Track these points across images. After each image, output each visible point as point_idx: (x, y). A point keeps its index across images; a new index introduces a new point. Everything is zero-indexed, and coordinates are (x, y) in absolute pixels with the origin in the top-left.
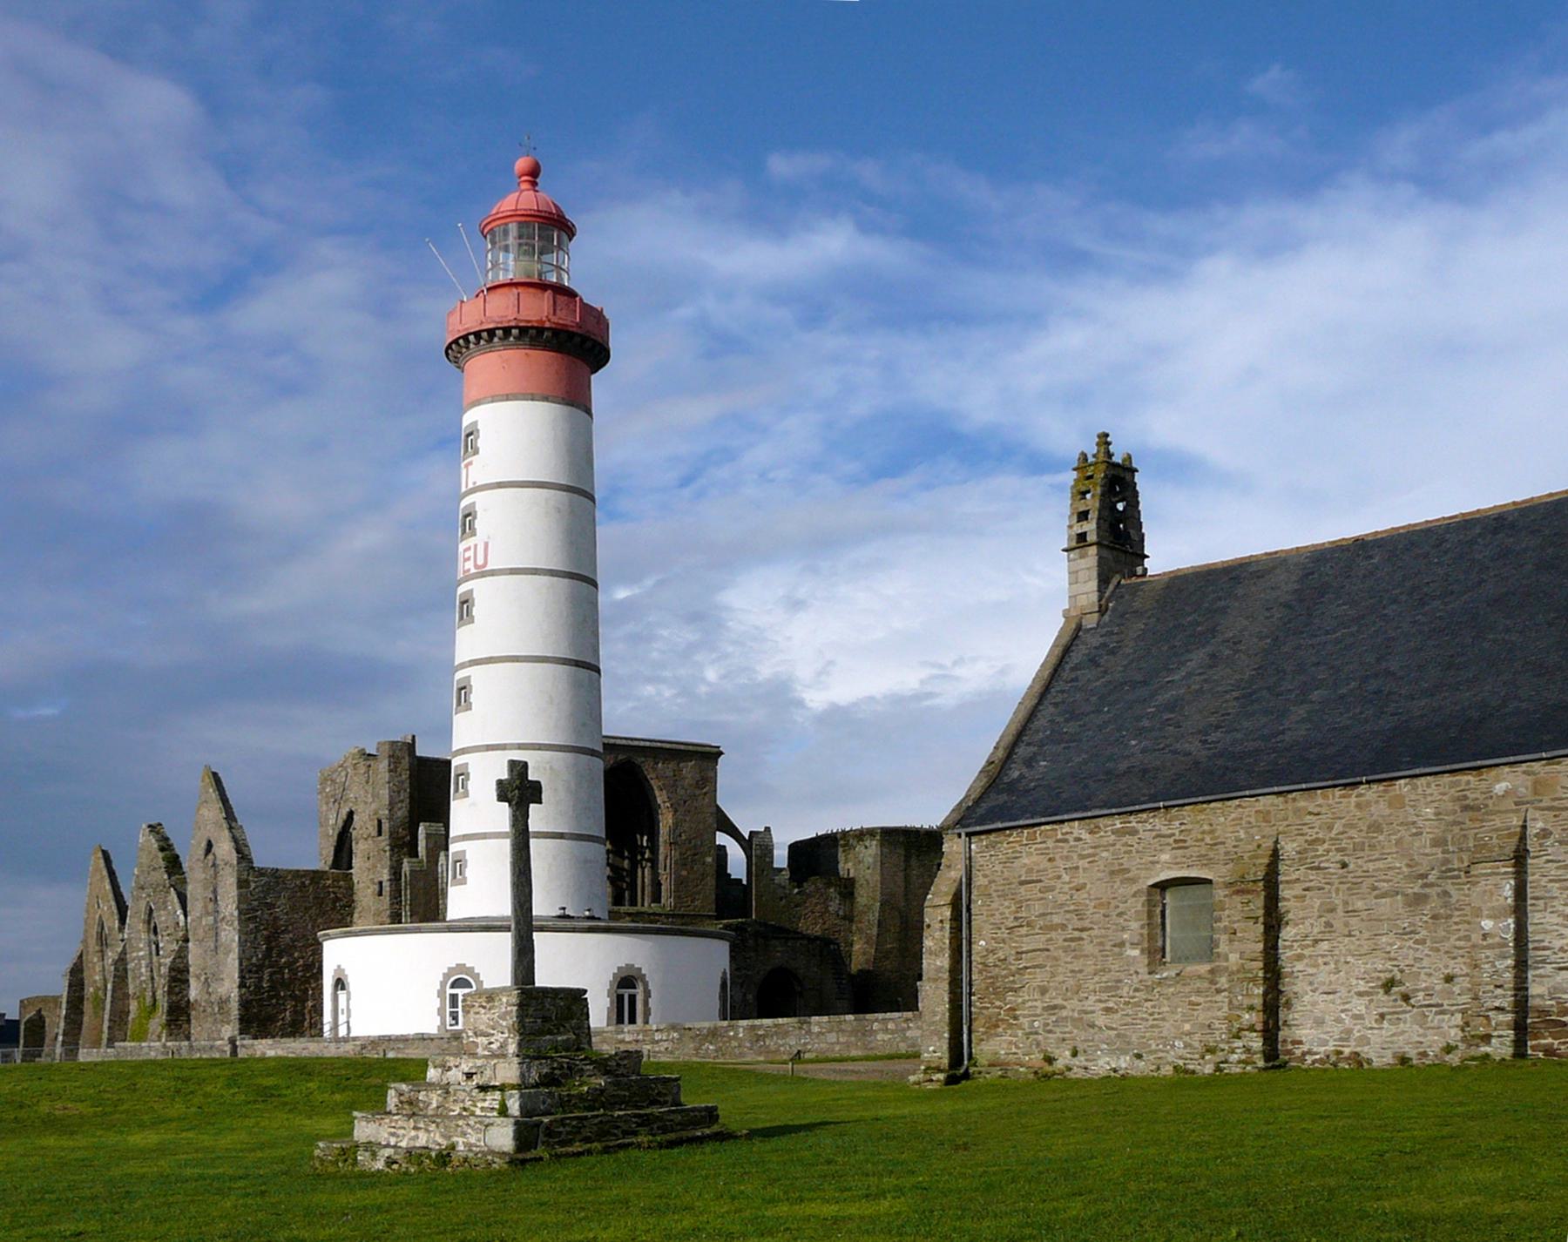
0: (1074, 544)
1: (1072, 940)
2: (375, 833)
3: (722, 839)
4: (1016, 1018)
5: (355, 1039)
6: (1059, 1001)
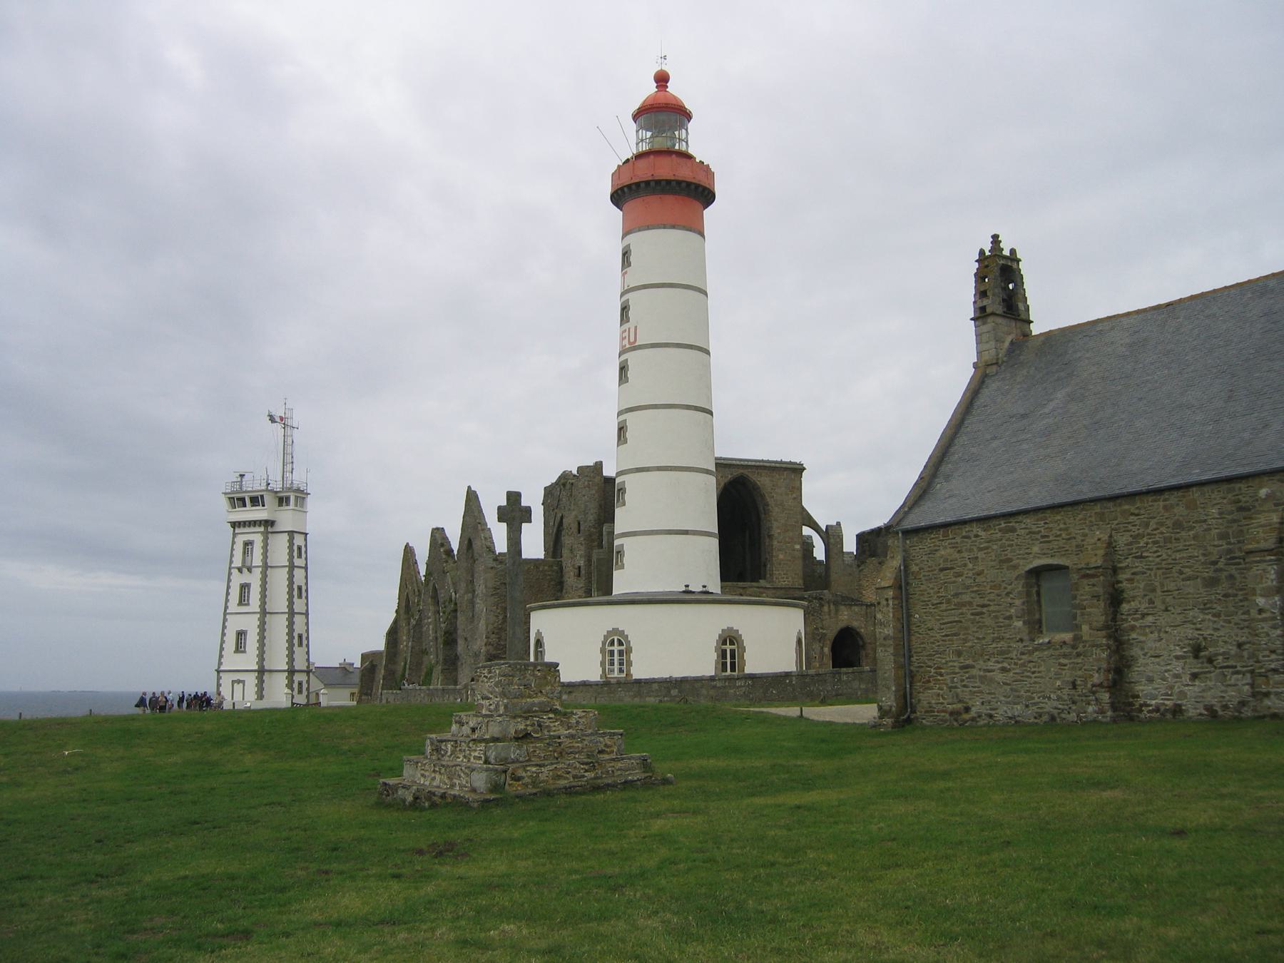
3: (807, 531)
4: (941, 675)
6: (969, 662)
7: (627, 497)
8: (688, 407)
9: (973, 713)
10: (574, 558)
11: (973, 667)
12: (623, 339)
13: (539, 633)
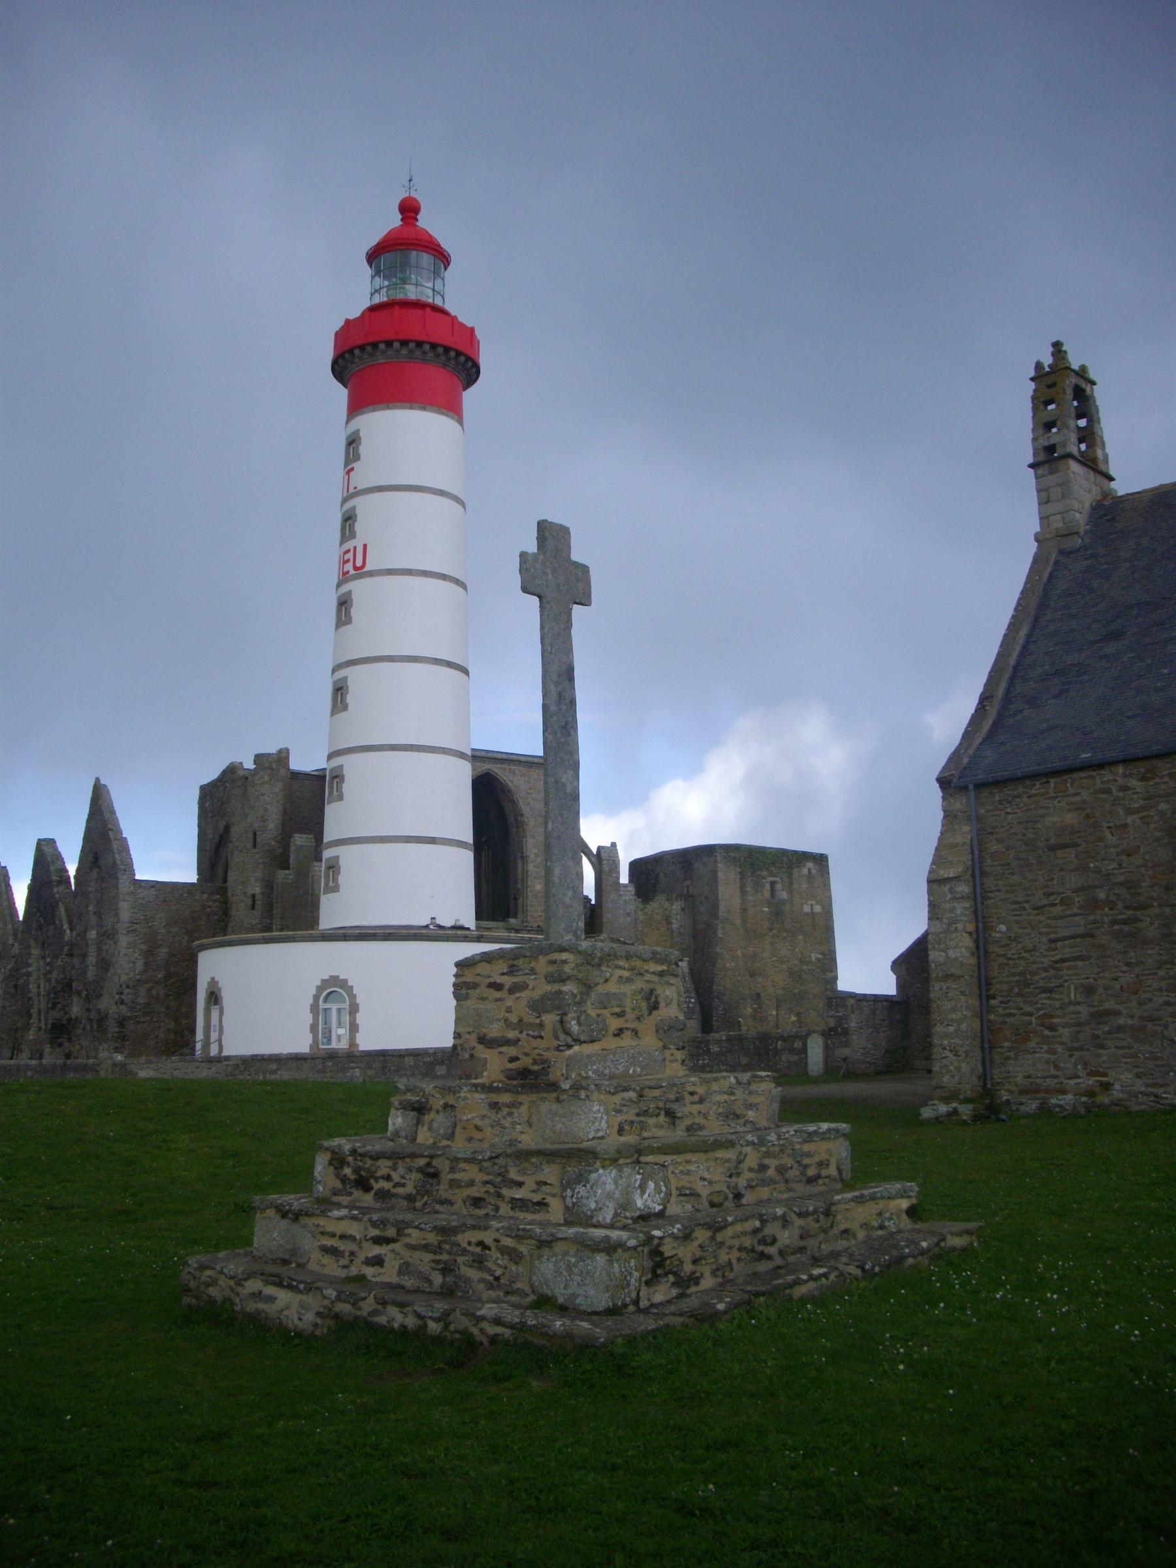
0: (1042, 458)
1: (1125, 922)
2: (249, 845)
4: (1052, 1028)
5: (227, 1058)
6: (1109, 1005)
7: (346, 788)
8: (449, 664)
9: (1117, 1092)
10: (247, 880)
11: (1117, 1013)
13: (213, 983)
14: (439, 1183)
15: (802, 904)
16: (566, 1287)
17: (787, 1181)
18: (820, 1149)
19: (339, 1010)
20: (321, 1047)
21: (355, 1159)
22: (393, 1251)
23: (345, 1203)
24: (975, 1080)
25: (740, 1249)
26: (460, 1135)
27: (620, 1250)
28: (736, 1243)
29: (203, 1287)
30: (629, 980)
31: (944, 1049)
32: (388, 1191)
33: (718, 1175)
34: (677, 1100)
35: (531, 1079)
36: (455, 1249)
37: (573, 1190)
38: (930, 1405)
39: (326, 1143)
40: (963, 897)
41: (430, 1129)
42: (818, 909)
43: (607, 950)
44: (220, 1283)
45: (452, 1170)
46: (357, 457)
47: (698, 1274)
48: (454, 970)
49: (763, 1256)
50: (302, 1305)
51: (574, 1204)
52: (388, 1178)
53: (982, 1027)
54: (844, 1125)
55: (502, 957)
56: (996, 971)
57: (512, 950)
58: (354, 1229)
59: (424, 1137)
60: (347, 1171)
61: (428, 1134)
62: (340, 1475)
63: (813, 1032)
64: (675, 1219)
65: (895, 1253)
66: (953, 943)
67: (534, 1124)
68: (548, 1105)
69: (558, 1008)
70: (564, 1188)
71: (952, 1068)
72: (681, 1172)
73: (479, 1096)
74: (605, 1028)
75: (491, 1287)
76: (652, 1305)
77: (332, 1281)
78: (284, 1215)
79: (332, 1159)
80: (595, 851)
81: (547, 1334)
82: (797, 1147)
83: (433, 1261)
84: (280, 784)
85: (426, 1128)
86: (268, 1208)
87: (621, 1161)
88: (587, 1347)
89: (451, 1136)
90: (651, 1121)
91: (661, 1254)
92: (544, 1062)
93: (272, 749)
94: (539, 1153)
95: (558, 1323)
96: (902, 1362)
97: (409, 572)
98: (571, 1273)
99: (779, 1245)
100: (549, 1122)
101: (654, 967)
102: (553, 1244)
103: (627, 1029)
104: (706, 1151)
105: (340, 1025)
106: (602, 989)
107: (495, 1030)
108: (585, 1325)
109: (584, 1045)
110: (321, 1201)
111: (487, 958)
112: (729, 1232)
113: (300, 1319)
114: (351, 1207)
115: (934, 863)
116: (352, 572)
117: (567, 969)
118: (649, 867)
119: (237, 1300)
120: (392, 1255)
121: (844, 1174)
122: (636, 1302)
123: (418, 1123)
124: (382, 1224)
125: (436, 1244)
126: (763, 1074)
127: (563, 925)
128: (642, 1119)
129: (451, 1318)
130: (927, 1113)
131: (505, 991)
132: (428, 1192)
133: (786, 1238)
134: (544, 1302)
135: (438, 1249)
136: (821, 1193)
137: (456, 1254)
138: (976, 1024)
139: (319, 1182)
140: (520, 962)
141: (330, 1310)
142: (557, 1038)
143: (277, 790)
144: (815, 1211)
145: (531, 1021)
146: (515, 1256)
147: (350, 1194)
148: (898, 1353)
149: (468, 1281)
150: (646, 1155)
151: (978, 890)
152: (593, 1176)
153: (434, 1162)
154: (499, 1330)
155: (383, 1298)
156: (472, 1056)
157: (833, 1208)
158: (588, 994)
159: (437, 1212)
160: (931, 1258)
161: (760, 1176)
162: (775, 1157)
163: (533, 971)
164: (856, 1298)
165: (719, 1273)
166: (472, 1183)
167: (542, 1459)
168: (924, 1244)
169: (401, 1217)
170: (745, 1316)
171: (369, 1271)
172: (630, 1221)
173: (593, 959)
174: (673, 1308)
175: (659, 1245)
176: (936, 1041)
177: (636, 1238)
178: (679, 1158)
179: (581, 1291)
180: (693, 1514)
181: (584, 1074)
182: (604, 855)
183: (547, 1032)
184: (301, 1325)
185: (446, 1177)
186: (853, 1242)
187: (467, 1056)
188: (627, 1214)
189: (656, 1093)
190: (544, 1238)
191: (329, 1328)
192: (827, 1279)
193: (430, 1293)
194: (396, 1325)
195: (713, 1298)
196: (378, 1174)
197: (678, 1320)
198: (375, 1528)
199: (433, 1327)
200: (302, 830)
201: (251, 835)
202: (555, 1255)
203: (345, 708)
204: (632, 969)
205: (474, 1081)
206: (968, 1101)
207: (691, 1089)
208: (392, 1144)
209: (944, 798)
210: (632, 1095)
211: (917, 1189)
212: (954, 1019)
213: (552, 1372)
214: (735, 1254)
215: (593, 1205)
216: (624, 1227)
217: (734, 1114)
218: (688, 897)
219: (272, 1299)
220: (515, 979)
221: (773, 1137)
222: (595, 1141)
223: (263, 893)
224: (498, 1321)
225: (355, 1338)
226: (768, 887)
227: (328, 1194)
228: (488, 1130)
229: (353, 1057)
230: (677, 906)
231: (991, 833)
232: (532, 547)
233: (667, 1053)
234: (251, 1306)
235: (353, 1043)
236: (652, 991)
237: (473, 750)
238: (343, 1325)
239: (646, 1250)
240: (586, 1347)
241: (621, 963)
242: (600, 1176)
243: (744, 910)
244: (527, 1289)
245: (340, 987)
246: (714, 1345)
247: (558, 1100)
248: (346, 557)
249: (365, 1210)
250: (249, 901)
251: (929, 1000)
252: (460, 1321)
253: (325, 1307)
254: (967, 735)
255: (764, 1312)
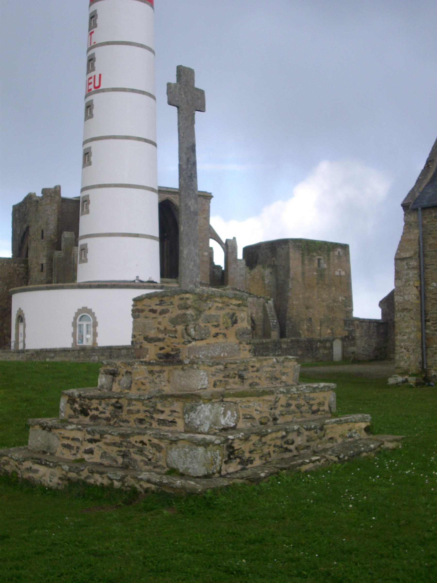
2: (39, 237)
3: (213, 243)
5: (27, 351)
7: (91, 207)
8: (146, 141)
10: (39, 256)
12: (90, 84)
13: (20, 311)
14: (122, 412)
15: (335, 271)
16: (184, 464)
17: (301, 412)
18: (319, 396)
19: (87, 325)
20: (78, 344)
21: (81, 400)
22: (98, 446)
23: (75, 422)
24: (418, 364)
25: (275, 446)
26: (134, 387)
27: (211, 446)
28: (273, 443)
29: (2, 466)
30: (221, 308)
31: (402, 347)
32: (97, 416)
33: (265, 408)
34: (245, 370)
35: (170, 359)
36: (129, 444)
37: (189, 415)
38: (362, 525)
39: (66, 392)
40: (413, 268)
41: (119, 384)
42: (343, 273)
43: (210, 293)
44: (11, 463)
45: (129, 404)
46: (95, 26)
47: (252, 459)
48: (132, 303)
49: (287, 450)
50: (52, 474)
51: (189, 422)
52: (97, 409)
53: (422, 337)
54: (333, 384)
55: (156, 296)
56: (430, 308)
57: (161, 292)
58: (79, 435)
59: (116, 388)
60: (77, 406)
61: (118, 387)
62: (61, 555)
63: (337, 338)
64: (241, 430)
65: (356, 450)
66: (407, 292)
67: (172, 381)
68: (178, 372)
69: (184, 322)
70: (184, 414)
71: (405, 358)
72: (245, 406)
73: (144, 367)
74: (209, 333)
75: (146, 464)
76: (228, 474)
77: (67, 462)
78: (44, 429)
79: (69, 400)
80: (224, 242)
81: (172, 487)
82: (307, 395)
83: (119, 451)
84: (56, 205)
85: (117, 383)
86: (36, 425)
87: (213, 400)
88: (192, 494)
89: (129, 388)
90: (231, 381)
91: (233, 448)
92: (178, 350)
93: (51, 186)
94: (172, 396)
95: (179, 482)
96: (352, 504)
97: (124, 90)
98: (186, 457)
99: (295, 444)
100: (178, 381)
101: (235, 302)
102: (178, 442)
103: (220, 333)
104: (258, 396)
105: (88, 332)
106: (207, 313)
107: (152, 334)
108: (192, 483)
109: (197, 341)
110: (63, 421)
111: (149, 296)
112: (269, 437)
113: (51, 481)
114: (77, 424)
115: (398, 249)
116: (93, 89)
117: (189, 302)
118: (253, 250)
119: (19, 472)
120: (98, 448)
121: (332, 409)
122: (219, 472)
123: (113, 382)
124: (92, 432)
125: (119, 442)
126: (291, 357)
127: (188, 280)
128: (226, 379)
129: (126, 480)
130: (391, 381)
131: (158, 313)
132: (116, 416)
133: (299, 441)
134: (173, 472)
135: (120, 445)
136: (320, 419)
137: (130, 447)
138: (419, 335)
139: (62, 412)
140: (165, 299)
141: (65, 476)
142: (183, 337)
143: (54, 208)
144: (315, 428)
145: (170, 329)
146: (159, 448)
147: (78, 417)
148: (351, 499)
149: (135, 461)
150: (227, 397)
151: (422, 264)
152: (199, 408)
153: (120, 401)
154: (149, 485)
155: (92, 470)
156: (141, 347)
157: (325, 427)
158: (200, 315)
159: (121, 426)
160: (376, 453)
161: (288, 409)
162: (295, 399)
163: (172, 303)
164: (334, 472)
165: (263, 458)
166: (138, 411)
167: (162, 548)
168: (372, 446)
169: (102, 429)
170: (275, 480)
171: (86, 457)
172: (217, 431)
173: (203, 297)
174: (238, 475)
175: (232, 443)
176: (397, 343)
177: (220, 439)
178: (244, 399)
179: (191, 466)
180: (232, 573)
181: (197, 356)
182: (229, 244)
183: (178, 335)
184: (51, 484)
185: (126, 408)
186: (335, 444)
187: (138, 346)
188: (216, 427)
189: (234, 366)
190: (173, 439)
191: (65, 486)
192: (320, 462)
193: (116, 467)
194: (98, 484)
195: (259, 471)
196: (92, 407)
197: (241, 481)
198: (75, 579)
199: (117, 484)
200: (68, 229)
201: (40, 232)
202: (178, 448)
203: (90, 164)
204: (223, 303)
205: (142, 360)
206: (413, 375)
207: (252, 364)
208: (99, 392)
209: (405, 215)
210: (221, 367)
211: (370, 418)
212: (407, 333)
213: (175, 506)
214: (272, 449)
215: (198, 423)
216: (215, 434)
217: (275, 377)
218: (274, 267)
219: (36, 471)
220: (163, 308)
221: (294, 389)
222: (202, 390)
223: (47, 263)
224: (149, 481)
225: (78, 491)
226: (316, 261)
227: (67, 417)
228: (148, 385)
229: (94, 350)
230: (268, 271)
231: (430, 234)
232: (174, 80)
233: (241, 346)
234: (26, 475)
235: (95, 342)
236: (234, 314)
237: (159, 187)
238: (72, 484)
239: (225, 445)
240: (192, 494)
241: (217, 300)
242: (202, 408)
243: (303, 273)
244: (165, 465)
245: (88, 313)
246: (258, 494)
247: (183, 369)
248: (90, 81)
249: (84, 426)
250: (40, 267)
251: (394, 322)
252: (130, 481)
253: (63, 475)
254: (419, 181)
255: (285, 477)
